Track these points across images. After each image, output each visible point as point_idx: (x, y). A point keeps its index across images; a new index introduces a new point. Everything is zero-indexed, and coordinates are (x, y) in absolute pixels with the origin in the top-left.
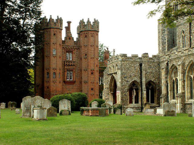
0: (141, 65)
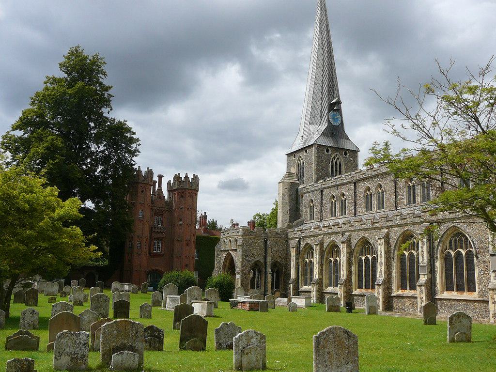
0: (266, 242)
